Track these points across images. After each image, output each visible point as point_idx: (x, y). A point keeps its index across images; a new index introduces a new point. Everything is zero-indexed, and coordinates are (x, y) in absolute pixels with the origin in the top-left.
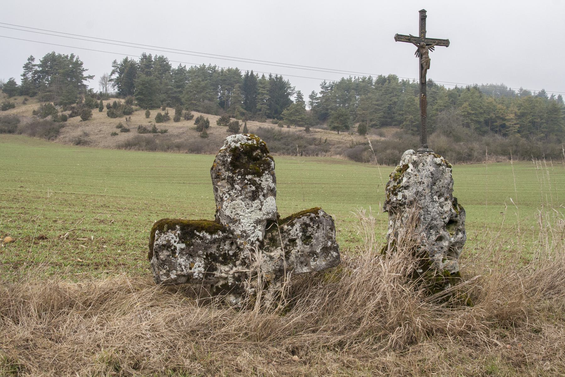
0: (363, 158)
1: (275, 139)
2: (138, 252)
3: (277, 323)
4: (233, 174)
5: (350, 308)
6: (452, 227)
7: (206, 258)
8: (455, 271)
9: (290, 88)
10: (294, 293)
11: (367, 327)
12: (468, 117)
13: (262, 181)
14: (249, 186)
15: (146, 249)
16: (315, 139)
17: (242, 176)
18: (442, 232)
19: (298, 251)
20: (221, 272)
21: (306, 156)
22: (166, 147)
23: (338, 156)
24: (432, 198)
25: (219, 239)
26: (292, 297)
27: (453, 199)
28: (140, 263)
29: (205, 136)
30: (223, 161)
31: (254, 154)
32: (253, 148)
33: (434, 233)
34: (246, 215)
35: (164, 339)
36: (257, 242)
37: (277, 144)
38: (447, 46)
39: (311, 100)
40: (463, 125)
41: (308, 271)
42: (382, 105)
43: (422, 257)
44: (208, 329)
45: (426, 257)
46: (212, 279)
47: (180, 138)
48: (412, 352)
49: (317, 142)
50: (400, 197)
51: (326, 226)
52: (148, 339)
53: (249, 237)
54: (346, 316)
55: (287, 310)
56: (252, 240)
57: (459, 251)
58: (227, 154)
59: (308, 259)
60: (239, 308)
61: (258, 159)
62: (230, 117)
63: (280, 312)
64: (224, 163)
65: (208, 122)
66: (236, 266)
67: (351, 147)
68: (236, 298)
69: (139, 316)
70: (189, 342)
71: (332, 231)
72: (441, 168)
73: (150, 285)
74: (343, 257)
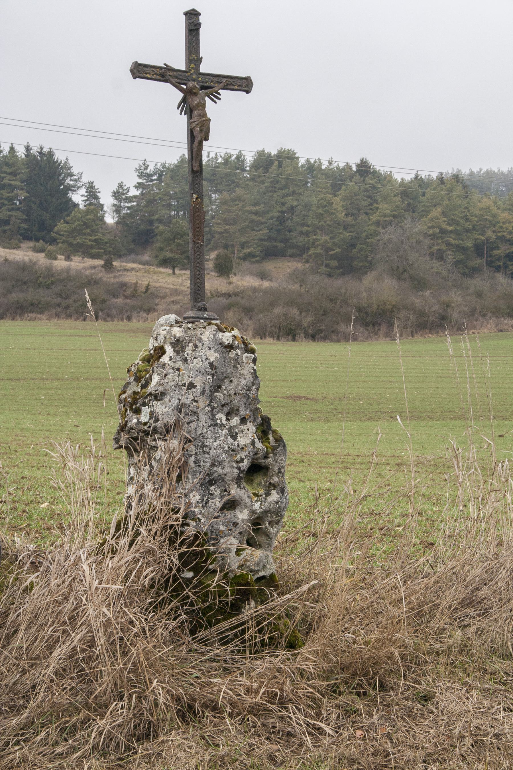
1: (40, 285)
6: (259, 479)
8: (266, 573)
9: (71, 175)
12: (442, 238)
16: (123, 285)
18: (234, 491)
21: (105, 320)
24: (213, 418)
27: (259, 420)
33: (218, 492)
38: (248, 92)
39: (116, 202)
40: (431, 255)
42: (265, 213)
43: (190, 545)
45: (198, 546)
48: (143, 757)
49: (129, 292)
50: (144, 417)
57: (272, 530)
72: (232, 354)
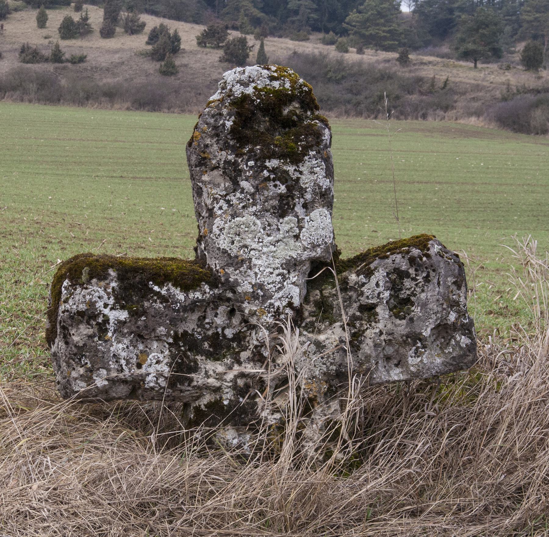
0: (533, 123)
1: (330, 80)
2: (21, 329)
3: (330, 492)
4: (237, 156)
5: (497, 465)
7: (174, 345)
10: (371, 426)
11: (538, 508)
13: (301, 173)
14: (272, 183)
15: (39, 321)
16: (420, 80)
17: (256, 161)
19: (381, 333)
20: (208, 376)
21: (398, 118)
22: (82, 94)
23: (473, 120)
25: (204, 300)
26: (366, 434)
28: (25, 353)
29: (169, 71)
30: (215, 128)
31: (286, 112)
32: (283, 98)
34: (265, 250)
35: (79, 520)
36: (288, 310)
37: (333, 91)
41: (402, 377)
44: (176, 500)
46: (187, 390)
47: (114, 75)
49: (426, 87)
51: (446, 277)
52: (43, 520)
53: (271, 297)
54: (489, 482)
55: (353, 465)
56: (277, 304)
58: (225, 111)
59: (402, 350)
60: (246, 456)
61: (294, 124)
62: (227, 28)
63: (338, 467)
64: (217, 132)
65: (176, 39)
66: (240, 363)
67: (504, 99)
68: (239, 435)
69: (24, 468)
70: (135, 528)
71: (459, 288)
73: (48, 400)
74: (484, 349)
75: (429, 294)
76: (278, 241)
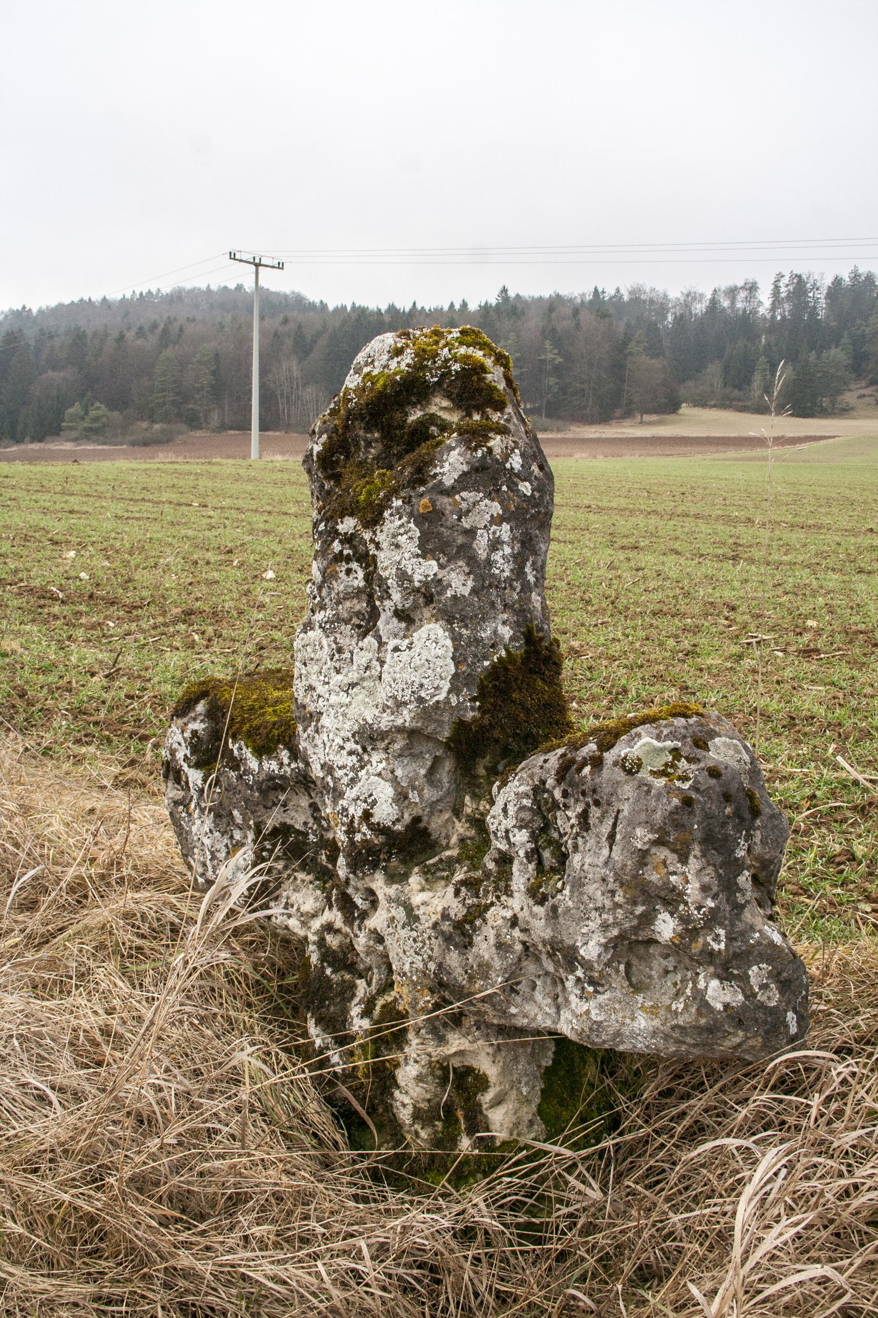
14: (344, 567)
51: (632, 824)
75: (588, 860)
76: (353, 685)
